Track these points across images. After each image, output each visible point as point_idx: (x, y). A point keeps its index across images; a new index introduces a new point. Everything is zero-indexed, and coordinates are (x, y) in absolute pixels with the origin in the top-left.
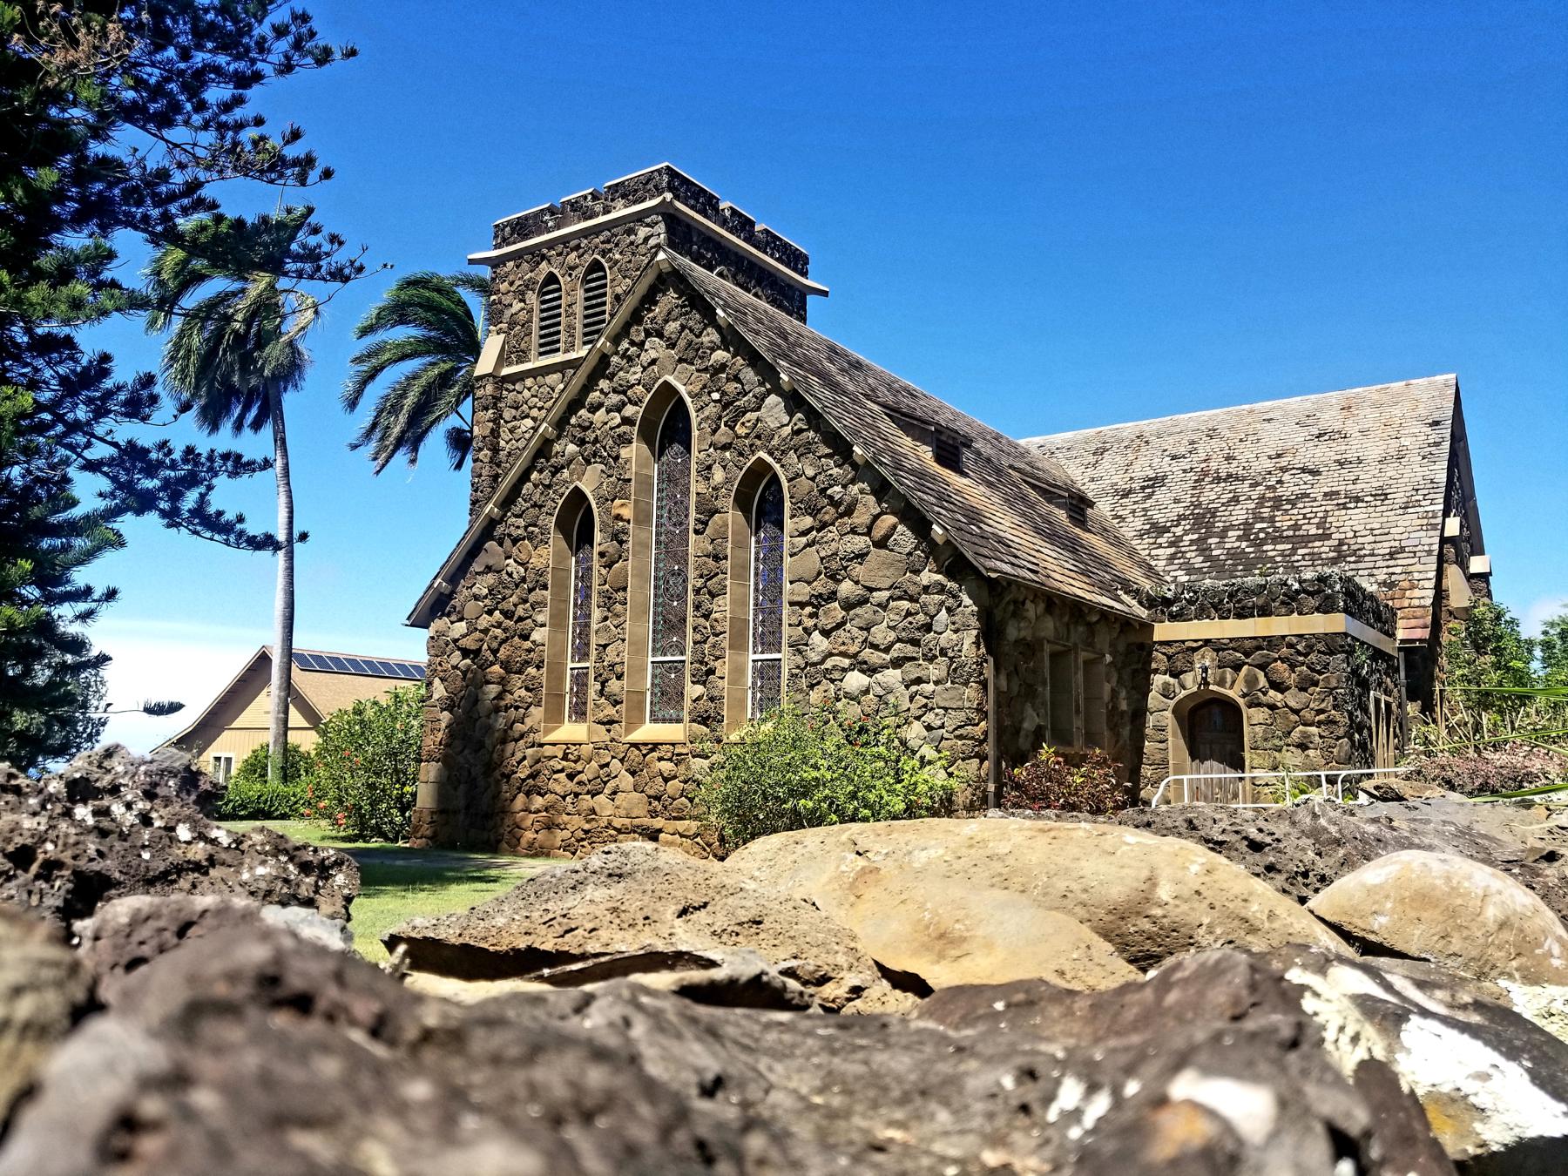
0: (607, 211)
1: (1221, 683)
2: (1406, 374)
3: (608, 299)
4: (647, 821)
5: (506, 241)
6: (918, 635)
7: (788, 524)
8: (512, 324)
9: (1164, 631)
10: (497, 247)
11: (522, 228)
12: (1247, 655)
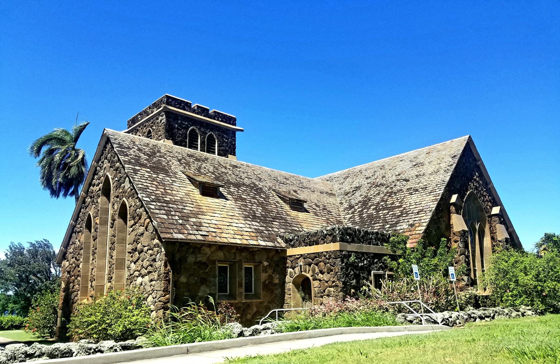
1: (305, 271)
2: (451, 138)
5: (130, 126)
6: (152, 263)
7: (128, 222)
9: (291, 252)
10: (128, 128)
11: (134, 121)
12: (313, 260)
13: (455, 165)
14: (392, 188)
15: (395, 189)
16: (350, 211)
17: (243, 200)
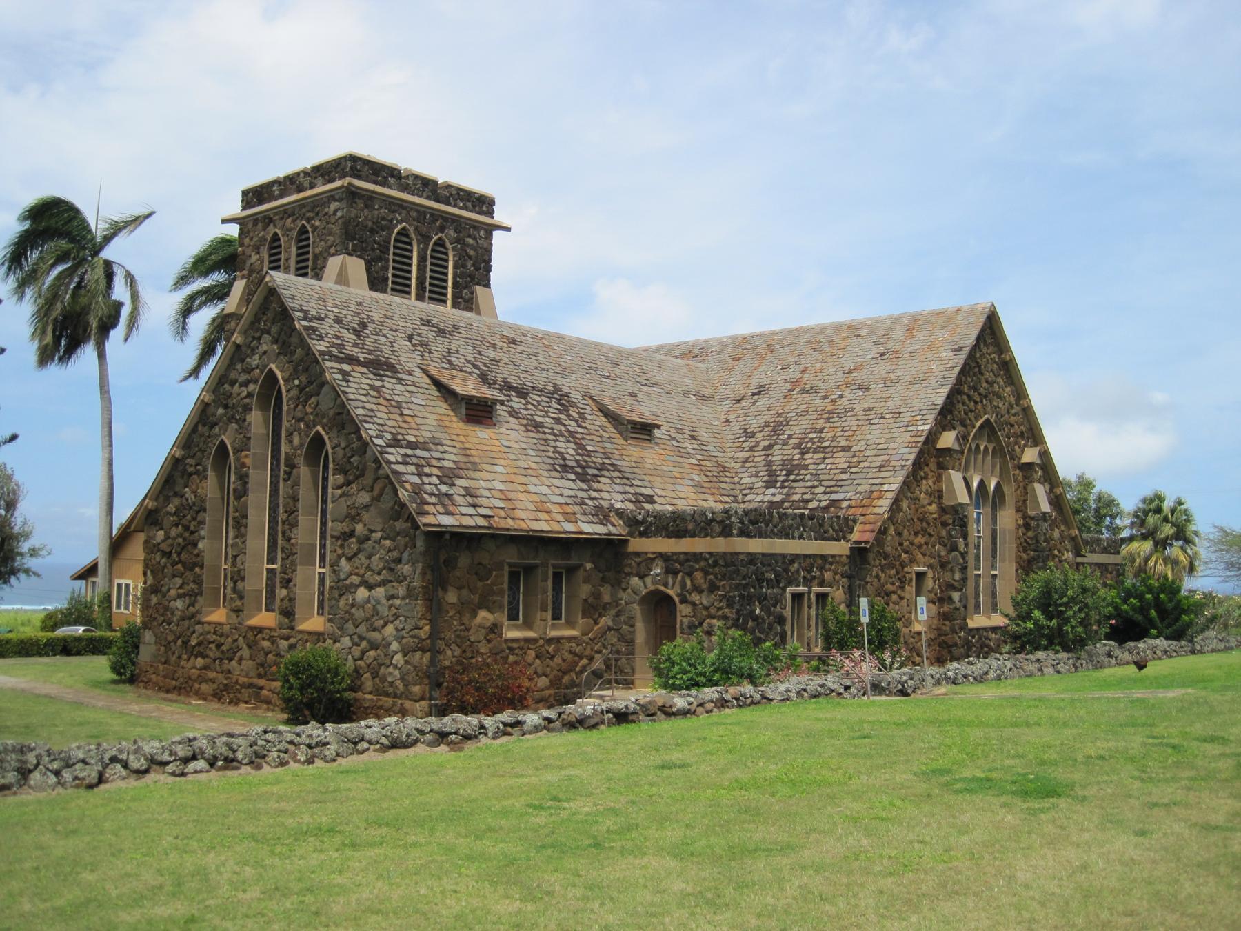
0: (312, 186)
3: (310, 256)
4: (255, 680)
6: (393, 565)
8: (251, 271)
9: (638, 544)
12: (681, 564)
13: (958, 369)
14: (834, 401)
15: (841, 406)
16: (745, 445)
17: (537, 426)
